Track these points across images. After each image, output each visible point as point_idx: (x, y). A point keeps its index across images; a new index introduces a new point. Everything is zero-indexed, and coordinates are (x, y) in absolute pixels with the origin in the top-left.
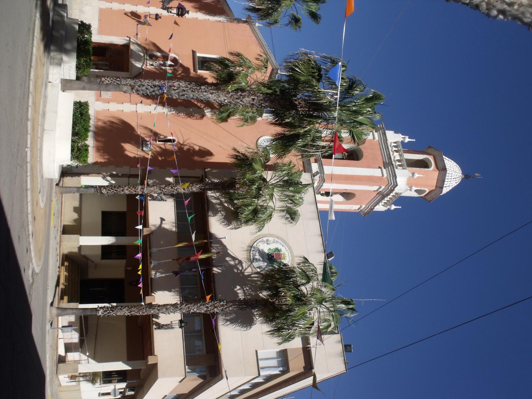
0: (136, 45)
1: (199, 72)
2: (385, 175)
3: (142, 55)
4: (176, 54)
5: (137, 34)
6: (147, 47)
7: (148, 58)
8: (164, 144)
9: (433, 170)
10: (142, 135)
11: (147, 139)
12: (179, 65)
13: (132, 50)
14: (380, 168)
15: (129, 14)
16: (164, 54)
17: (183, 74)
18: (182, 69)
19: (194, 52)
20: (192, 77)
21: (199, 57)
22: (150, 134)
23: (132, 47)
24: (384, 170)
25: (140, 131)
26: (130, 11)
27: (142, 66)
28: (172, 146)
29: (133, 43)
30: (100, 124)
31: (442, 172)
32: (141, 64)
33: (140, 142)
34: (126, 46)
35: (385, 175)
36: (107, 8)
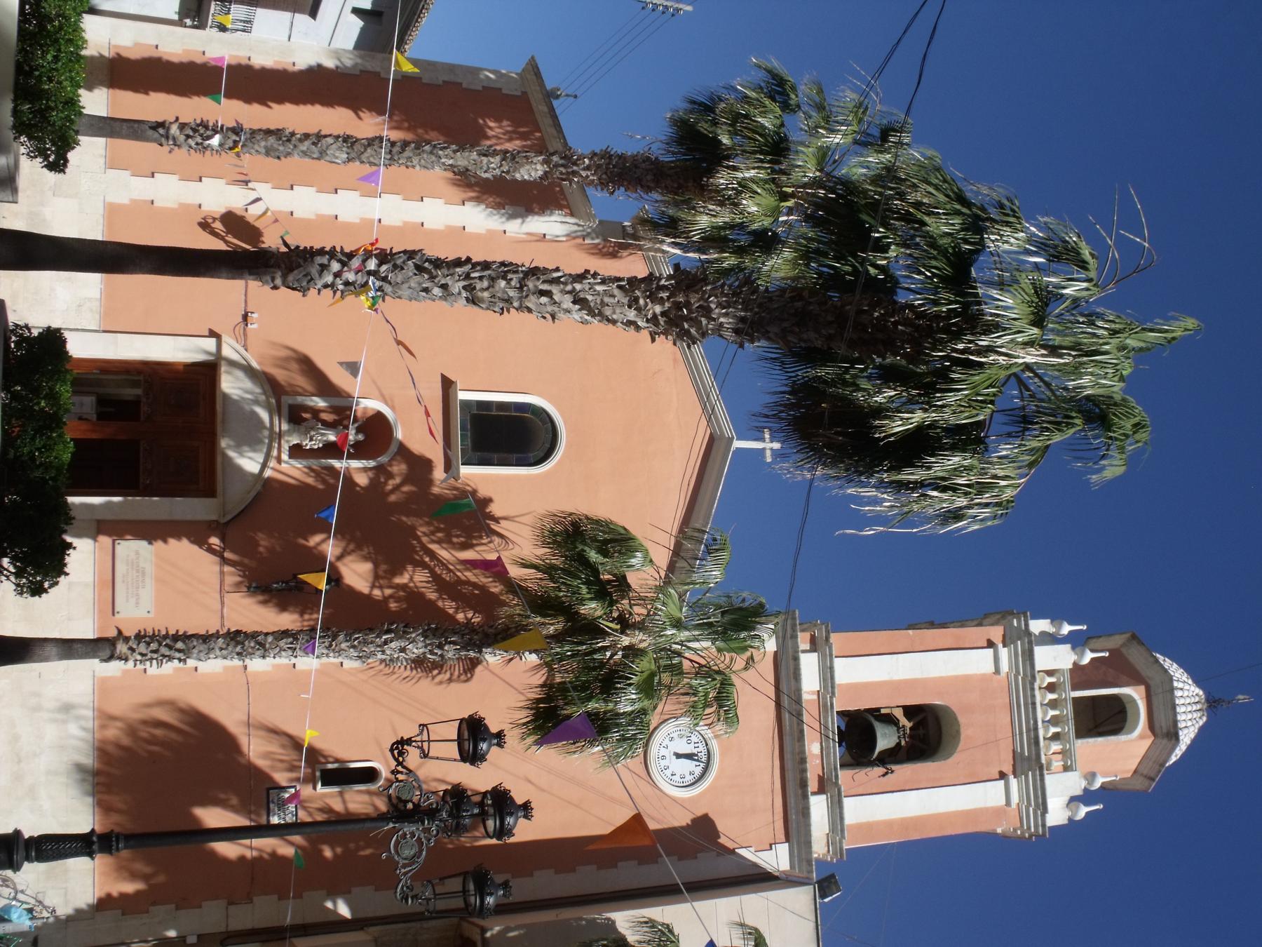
0: (240, 374)
1: (465, 470)
2: (1015, 798)
3: (264, 415)
4: (386, 403)
5: (245, 317)
6: (280, 375)
7: (285, 427)
8: (341, 793)
9: (1141, 737)
10: (261, 763)
11: (281, 778)
12: (393, 448)
13: (226, 397)
14: (1002, 776)
15: (218, 226)
16: (338, 402)
17: (406, 489)
18: (403, 467)
19: (448, 385)
20: (438, 497)
21: (466, 404)
22: (290, 755)
23: (232, 385)
24: (1013, 782)
25: (256, 750)
26: (223, 210)
27: (264, 466)
28: (366, 798)
29: (232, 363)
30: (113, 733)
31: (1165, 741)
32: (260, 458)
33: (256, 790)
34: (207, 372)
35: (1015, 798)
36: (134, 202)
